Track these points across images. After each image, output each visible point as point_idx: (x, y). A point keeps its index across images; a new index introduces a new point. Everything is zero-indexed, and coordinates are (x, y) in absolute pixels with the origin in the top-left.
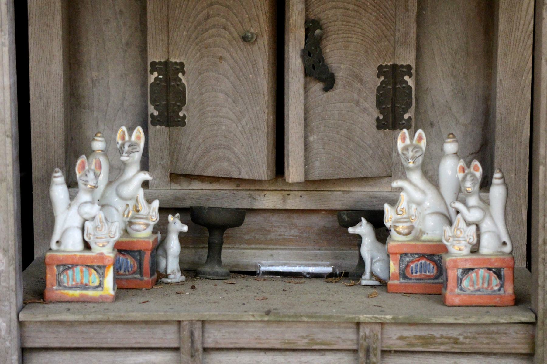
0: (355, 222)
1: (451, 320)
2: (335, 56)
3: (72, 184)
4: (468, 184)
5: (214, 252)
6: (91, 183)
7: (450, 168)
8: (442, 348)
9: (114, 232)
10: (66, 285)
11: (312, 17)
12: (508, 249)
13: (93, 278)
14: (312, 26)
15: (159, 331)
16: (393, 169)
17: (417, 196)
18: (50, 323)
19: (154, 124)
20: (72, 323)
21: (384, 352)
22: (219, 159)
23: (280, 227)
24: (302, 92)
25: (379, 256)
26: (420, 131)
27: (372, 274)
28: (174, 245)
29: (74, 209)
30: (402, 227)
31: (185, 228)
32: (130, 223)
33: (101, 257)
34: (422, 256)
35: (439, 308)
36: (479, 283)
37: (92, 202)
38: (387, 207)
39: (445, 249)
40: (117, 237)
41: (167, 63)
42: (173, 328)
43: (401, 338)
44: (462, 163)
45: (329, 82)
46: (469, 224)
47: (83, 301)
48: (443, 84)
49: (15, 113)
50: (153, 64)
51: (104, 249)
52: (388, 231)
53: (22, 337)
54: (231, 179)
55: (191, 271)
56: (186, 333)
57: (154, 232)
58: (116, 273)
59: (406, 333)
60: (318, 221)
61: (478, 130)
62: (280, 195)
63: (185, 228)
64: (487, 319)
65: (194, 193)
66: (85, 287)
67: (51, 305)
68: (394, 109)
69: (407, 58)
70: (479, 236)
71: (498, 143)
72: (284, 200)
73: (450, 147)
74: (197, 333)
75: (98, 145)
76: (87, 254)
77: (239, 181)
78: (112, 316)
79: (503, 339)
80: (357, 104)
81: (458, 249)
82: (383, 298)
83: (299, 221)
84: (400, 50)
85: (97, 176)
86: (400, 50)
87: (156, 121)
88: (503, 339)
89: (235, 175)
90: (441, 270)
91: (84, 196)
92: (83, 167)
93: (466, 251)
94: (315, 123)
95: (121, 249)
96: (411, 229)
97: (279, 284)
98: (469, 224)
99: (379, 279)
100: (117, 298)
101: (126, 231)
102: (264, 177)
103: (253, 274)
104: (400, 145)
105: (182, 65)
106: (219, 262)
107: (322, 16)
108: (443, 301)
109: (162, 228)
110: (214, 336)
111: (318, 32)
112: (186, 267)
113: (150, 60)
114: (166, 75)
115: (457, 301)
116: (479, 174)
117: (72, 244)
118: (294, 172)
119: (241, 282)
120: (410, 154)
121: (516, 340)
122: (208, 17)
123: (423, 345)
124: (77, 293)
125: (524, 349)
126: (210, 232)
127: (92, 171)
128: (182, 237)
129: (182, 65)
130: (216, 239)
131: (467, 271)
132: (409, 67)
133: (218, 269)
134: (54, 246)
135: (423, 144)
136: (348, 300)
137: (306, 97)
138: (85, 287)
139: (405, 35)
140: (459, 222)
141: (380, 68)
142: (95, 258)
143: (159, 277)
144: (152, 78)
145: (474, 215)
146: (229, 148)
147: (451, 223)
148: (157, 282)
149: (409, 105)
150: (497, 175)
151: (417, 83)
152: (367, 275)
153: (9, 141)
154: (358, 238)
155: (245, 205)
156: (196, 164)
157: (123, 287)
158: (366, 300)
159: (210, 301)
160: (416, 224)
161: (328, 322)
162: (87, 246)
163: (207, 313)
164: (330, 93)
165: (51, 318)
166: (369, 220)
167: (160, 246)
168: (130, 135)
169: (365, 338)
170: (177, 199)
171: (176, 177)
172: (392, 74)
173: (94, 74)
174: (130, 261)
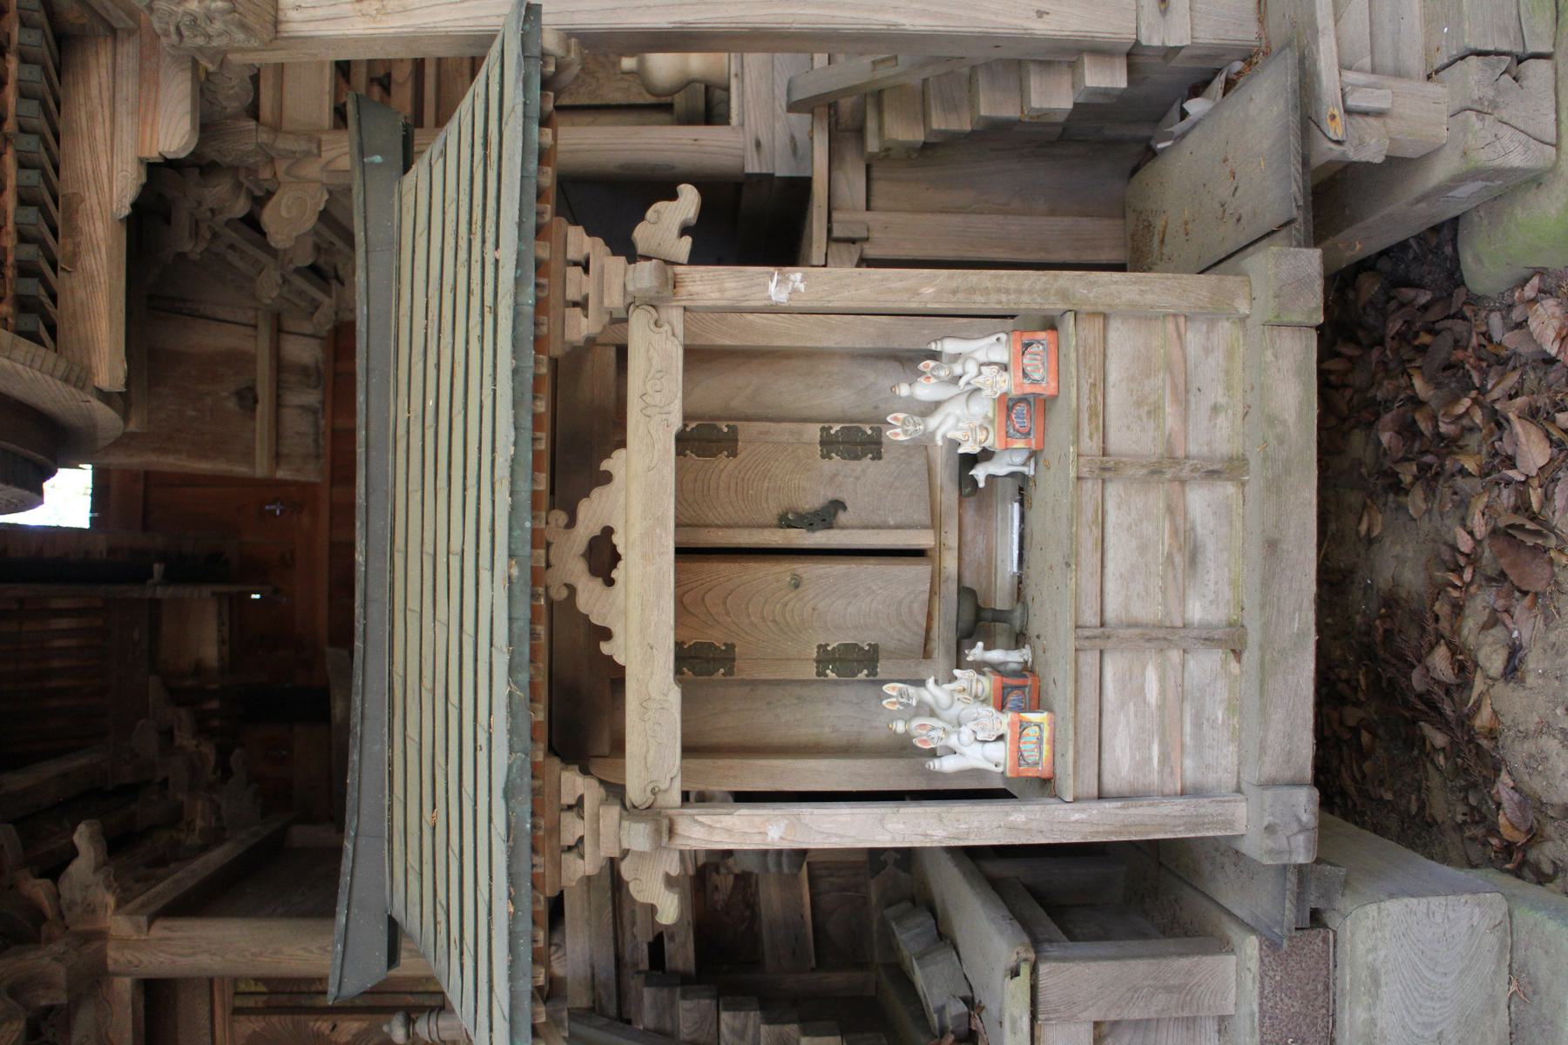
0: (975, 482)
1: (1074, 390)
2: (812, 501)
3: (933, 754)
4: (943, 373)
5: (1001, 616)
6: (941, 733)
7: (925, 390)
8: (1100, 399)
9: (988, 711)
10: (1038, 757)
11: (775, 522)
12: (1003, 337)
13: (1032, 732)
14: (785, 522)
15: (1085, 669)
16: (922, 445)
17: (951, 421)
18: (1075, 773)
19: (875, 674)
20: (1076, 752)
21: (1104, 454)
22: (911, 613)
23: (976, 550)
24: (847, 532)
25: (1007, 458)
26: (889, 419)
27: (1024, 464)
28: (996, 655)
29: (964, 750)
30: (981, 436)
31: (980, 644)
32: (976, 697)
33: (1011, 724)
34: (1009, 417)
35: (1060, 401)
36: (1037, 364)
37: (959, 733)
38: (961, 450)
39: (1005, 394)
40: (992, 709)
41: (818, 661)
42: (1082, 655)
43: (1091, 437)
44: (922, 379)
45: (838, 505)
46: (980, 373)
47: (1053, 742)
48: (839, 397)
49: (875, 804)
50: (818, 674)
51: (1004, 722)
52: (984, 450)
53: (1088, 799)
54: (930, 600)
55: (1019, 639)
56: (1087, 643)
57: (984, 674)
58: (1024, 710)
59: (1087, 433)
60: (970, 516)
61: (882, 365)
62: (944, 553)
63: (980, 644)
64: (1073, 356)
65: (943, 633)
66: (1040, 739)
67: (1058, 771)
68: (862, 443)
69: (814, 431)
70: (990, 364)
71: (896, 345)
72: (949, 549)
73: (904, 390)
74: (1087, 633)
75: (900, 727)
76: (1008, 738)
77: (932, 593)
78: (1070, 714)
79: (1091, 341)
80: (857, 478)
81: (1005, 383)
82: (1051, 453)
83: (969, 537)
84: (806, 438)
85: (933, 729)
86: (806, 438)
87: (873, 672)
88: (1091, 341)
89: (926, 596)
90: (1023, 399)
91: (953, 741)
92: (924, 741)
93: (1006, 375)
94: (877, 520)
95: (1002, 707)
96: (982, 427)
97: (1032, 555)
98: (980, 373)
99: (1029, 458)
100: (1050, 710)
101: (983, 701)
102: (929, 568)
103: (1020, 578)
104: (902, 438)
105: (819, 647)
106: (1011, 612)
107: (775, 512)
108: (1054, 398)
109: (979, 667)
110: (1090, 617)
111: (790, 516)
112: (1013, 643)
113: (815, 677)
114: (829, 662)
115: (1053, 384)
116: (932, 363)
117: (999, 752)
118: (923, 539)
119: (1030, 591)
120: (911, 428)
121: (1091, 330)
122: (774, 621)
123: (1097, 416)
124: (1046, 748)
125: (1099, 322)
126: (979, 620)
127: (926, 733)
128: (987, 648)
129: (819, 647)
130: (989, 615)
131: (1025, 375)
132: (823, 429)
133: (1018, 613)
134: (1000, 769)
135: (901, 416)
136: (1051, 490)
137: (852, 527)
138: (1040, 739)
139: (792, 433)
140: (977, 383)
141: (823, 457)
142: (1013, 732)
143: (1026, 670)
144: (831, 675)
145: (972, 368)
146: (900, 603)
147: (979, 390)
148: (1032, 671)
149: (715, 427)
150: (933, 346)
151: (837, 421)
152: (1025, 469)
153: (902, 810)
154: (991, 478)
155: (953, 587)
156: (915, 633)
157: (1037, 704)
158: (1052, 471)
159: (1054, 619)
160: (978, 423)
161: (1077, 507)
162: (1001, 738)
163: (1070, 624)
164: (848, 504)
165: (1070, 770)
166: (972, 468)
167: (996, 668)
168: (890, 696)
169: (1091, 471)
170: (948, 652)
171: (927, 654)
172: (828, 444)
173: (827, 730)
174: (1013, 698)
